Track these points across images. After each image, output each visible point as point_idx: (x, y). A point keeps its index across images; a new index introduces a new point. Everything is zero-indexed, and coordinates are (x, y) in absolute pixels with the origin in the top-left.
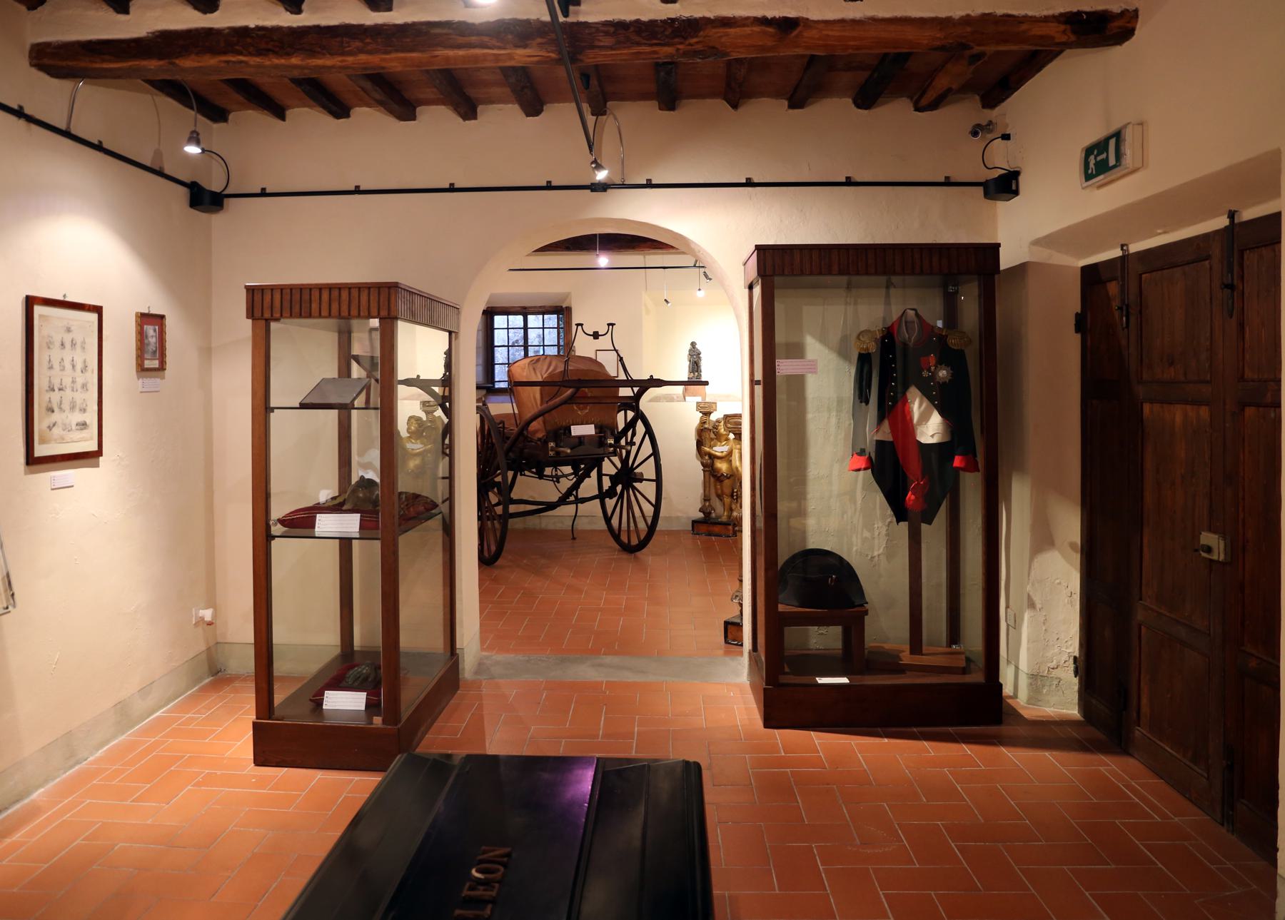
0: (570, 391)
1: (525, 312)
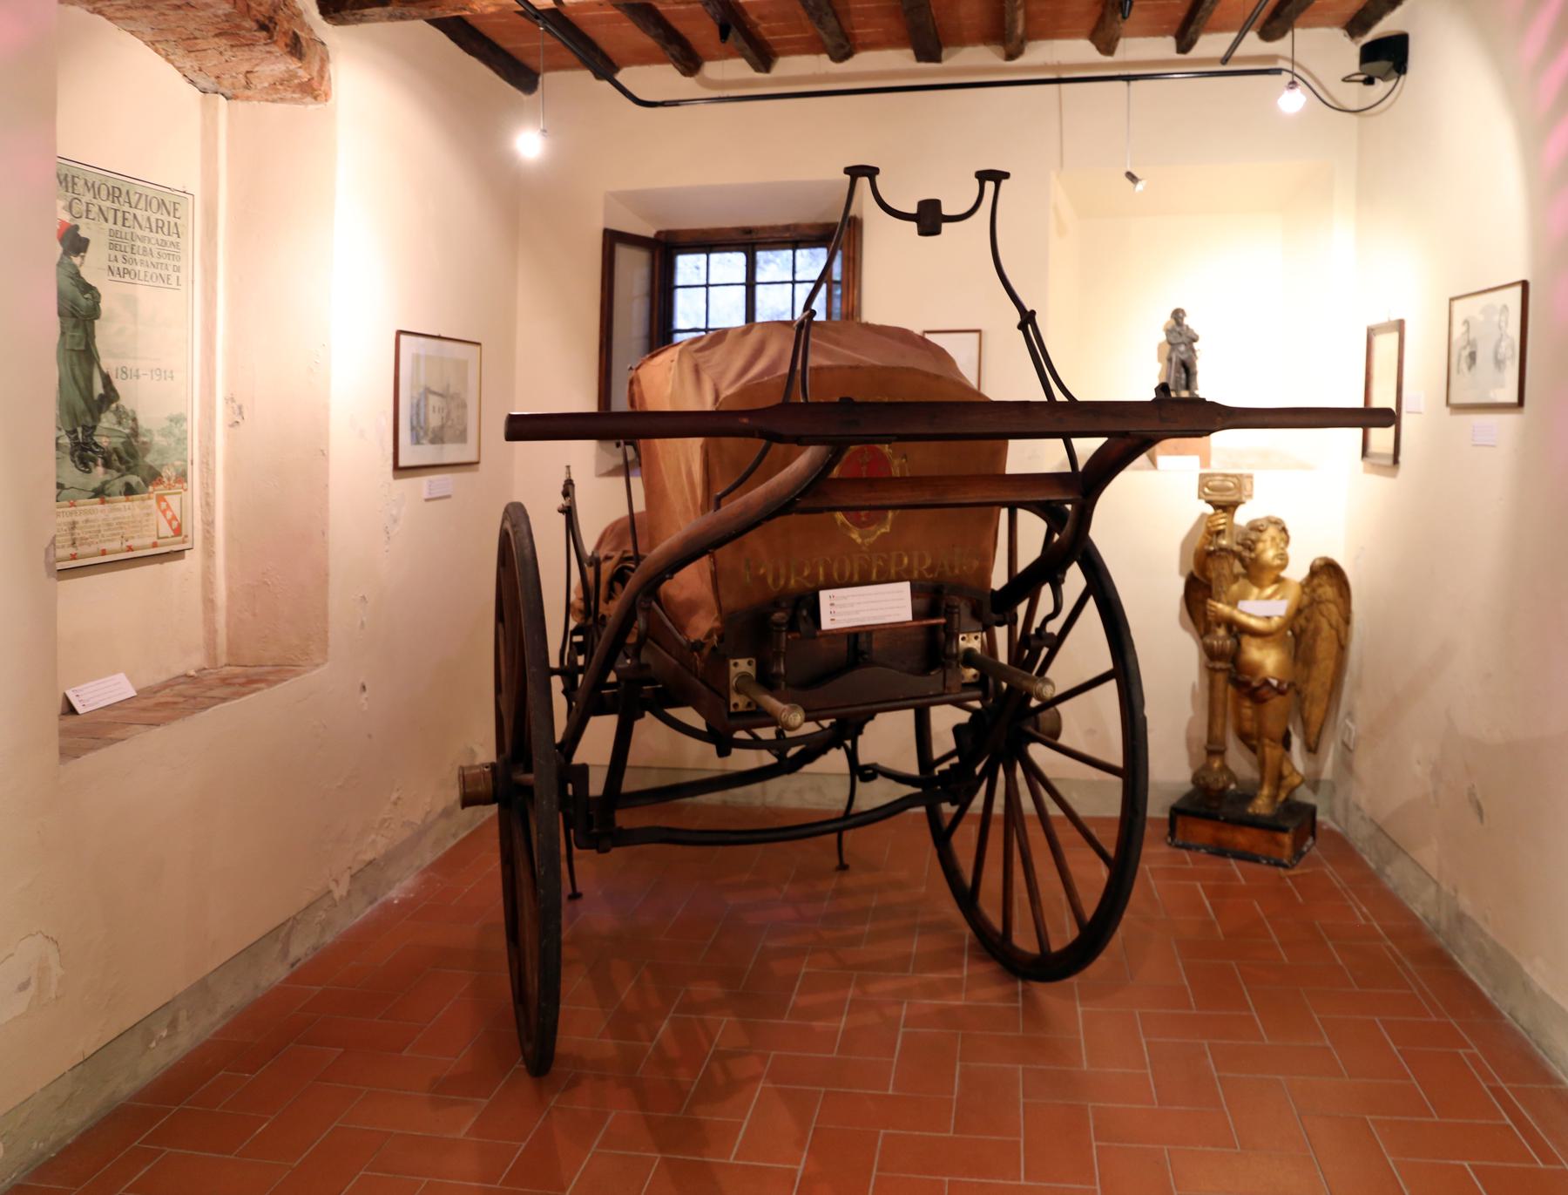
0: (804, 460)
1: (749, 242)
